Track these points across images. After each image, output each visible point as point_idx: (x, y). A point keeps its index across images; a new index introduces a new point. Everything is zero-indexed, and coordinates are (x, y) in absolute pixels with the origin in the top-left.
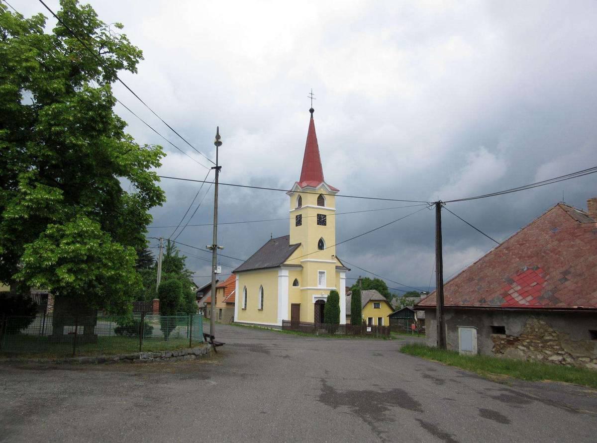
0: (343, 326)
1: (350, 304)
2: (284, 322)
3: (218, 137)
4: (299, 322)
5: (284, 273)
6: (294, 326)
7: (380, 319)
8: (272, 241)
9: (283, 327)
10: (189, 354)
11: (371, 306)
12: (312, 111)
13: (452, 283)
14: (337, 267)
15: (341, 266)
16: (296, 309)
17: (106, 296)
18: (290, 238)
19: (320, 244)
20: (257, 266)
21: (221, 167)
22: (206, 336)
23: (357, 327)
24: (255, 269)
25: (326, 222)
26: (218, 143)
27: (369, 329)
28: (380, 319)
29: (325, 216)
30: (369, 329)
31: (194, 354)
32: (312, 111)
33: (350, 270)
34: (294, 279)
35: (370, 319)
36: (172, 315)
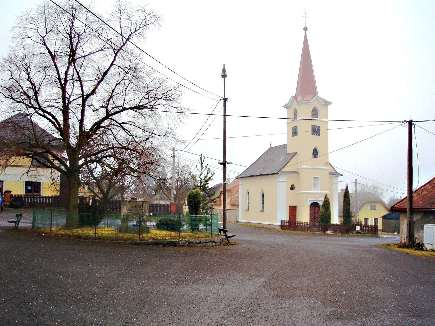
0: (334, 225)
1: (342, 207)
2: (282, 222)
3: (224, 71)
4: (295, 222)
5: (281, 178)
6: (292, 224)
7: (376, 220)
8: (271, 150)
9: (282, 227)
10: (211, 242)
11: (367, 207)
12: (305, 29)
13: (423, 188)
14: (330, 173)
15: (335, 171)
16: (293, 210)
17: (208, 209)
18: (287, 147)
19: (315, 153)
20: (258, 173)
21: (227, 98)
22: (220, 230)
23: (348, 226)
24: (257, 176)
25: (319, 132)
26: (224, 76)
27: (358, 228)
28: (376, 220)
29: (319, 127)
30: (358, 228)
31: (214, 242)
32: (305, 29)
33: (342, 175)
34: (291, 185)
35: (366, 220)
36: (196, 214)
